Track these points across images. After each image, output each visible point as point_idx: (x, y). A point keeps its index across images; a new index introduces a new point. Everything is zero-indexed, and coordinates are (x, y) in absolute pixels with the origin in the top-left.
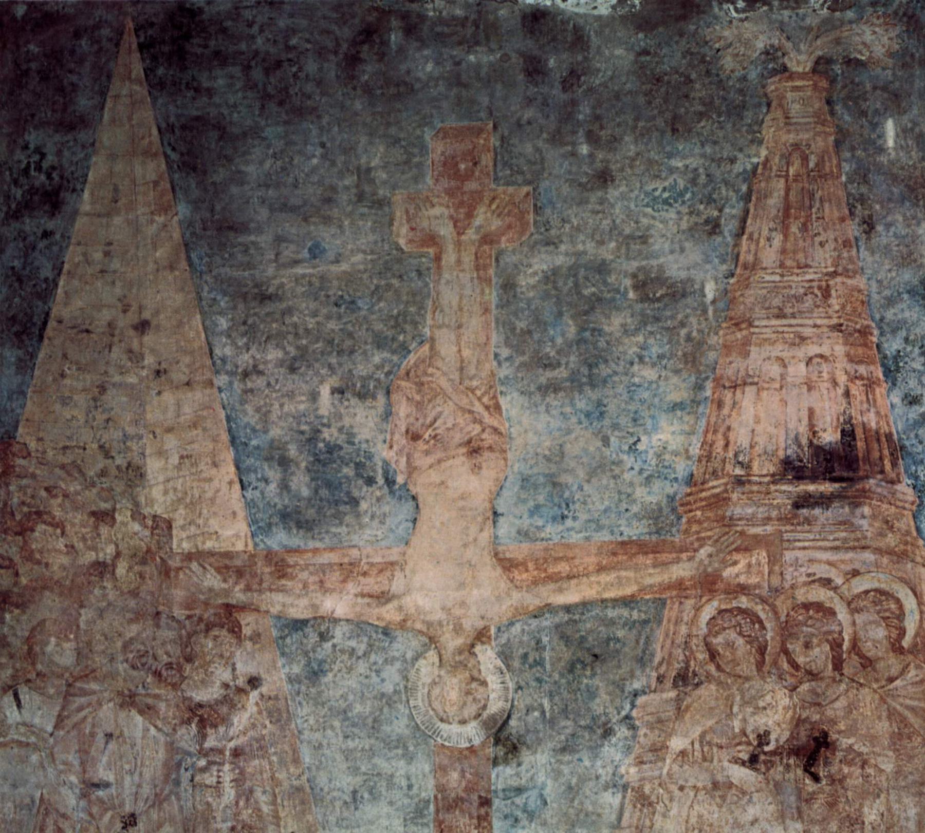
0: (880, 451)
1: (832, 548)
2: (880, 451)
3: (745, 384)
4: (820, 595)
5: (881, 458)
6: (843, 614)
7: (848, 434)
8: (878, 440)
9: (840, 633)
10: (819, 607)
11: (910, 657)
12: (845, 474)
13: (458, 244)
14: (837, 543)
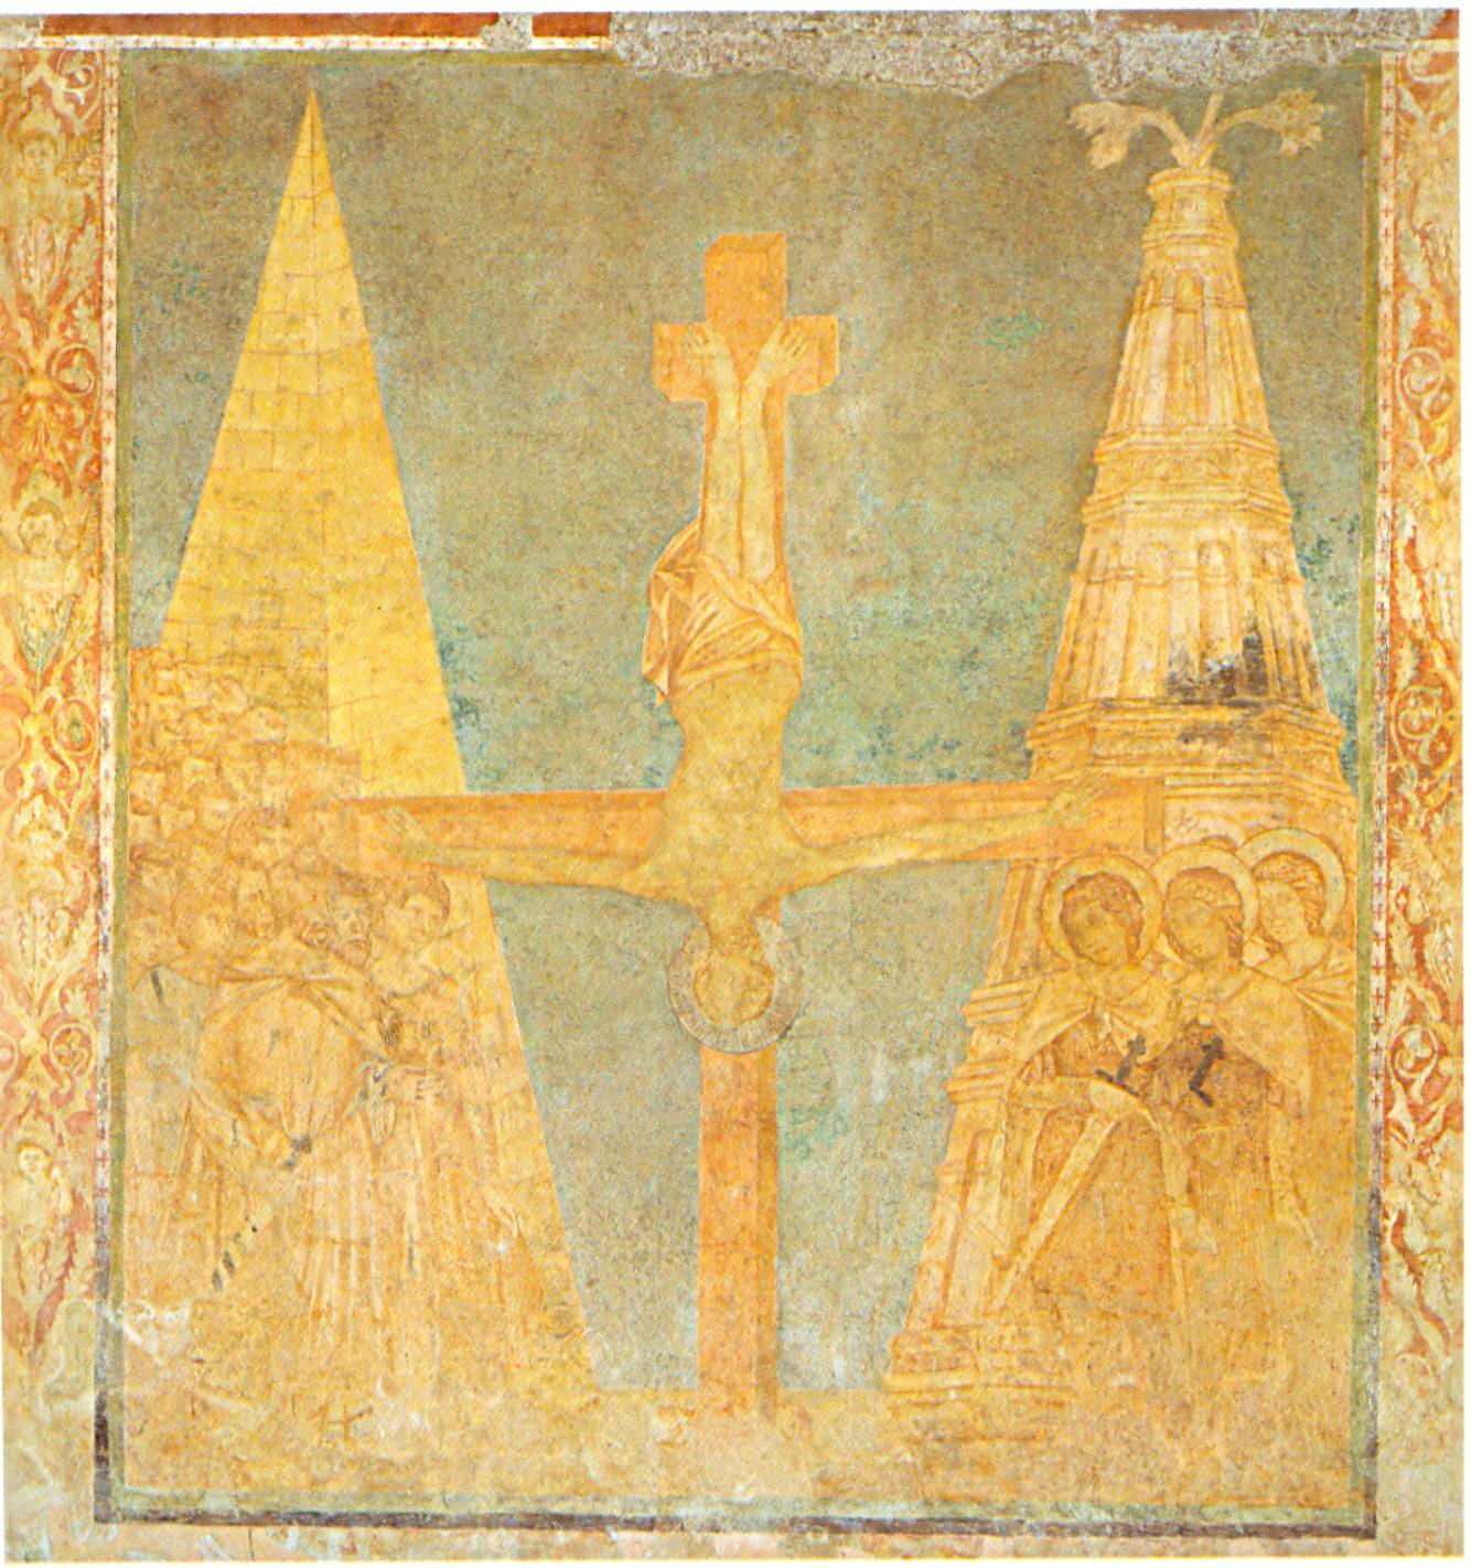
0: (1296, 666)
1: (1228, 796)
2: (1296, 666)
3: (1118, 578)
4: (1217, 859)
5: (1296, 678)
6: (1243, 882)
7: (1253, 646)
8: (1294, 655)
9: (1241, 907)
10: (1210, 872)
11: (1334, 941)
12: (1248, 698)
13: (741, 389)
14: (1238, 790)
